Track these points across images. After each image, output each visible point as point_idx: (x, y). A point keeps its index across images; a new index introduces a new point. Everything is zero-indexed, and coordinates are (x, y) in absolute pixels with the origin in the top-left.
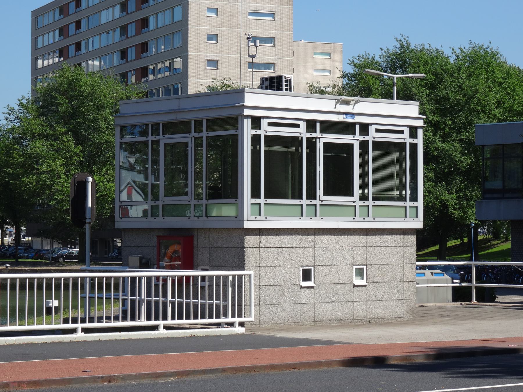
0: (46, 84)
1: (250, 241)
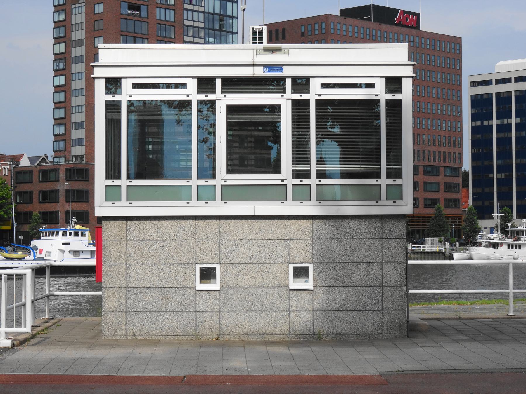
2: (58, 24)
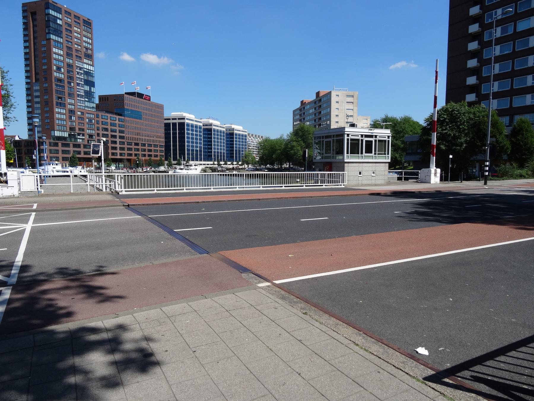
0: (296, 129)
1: (346, 165)
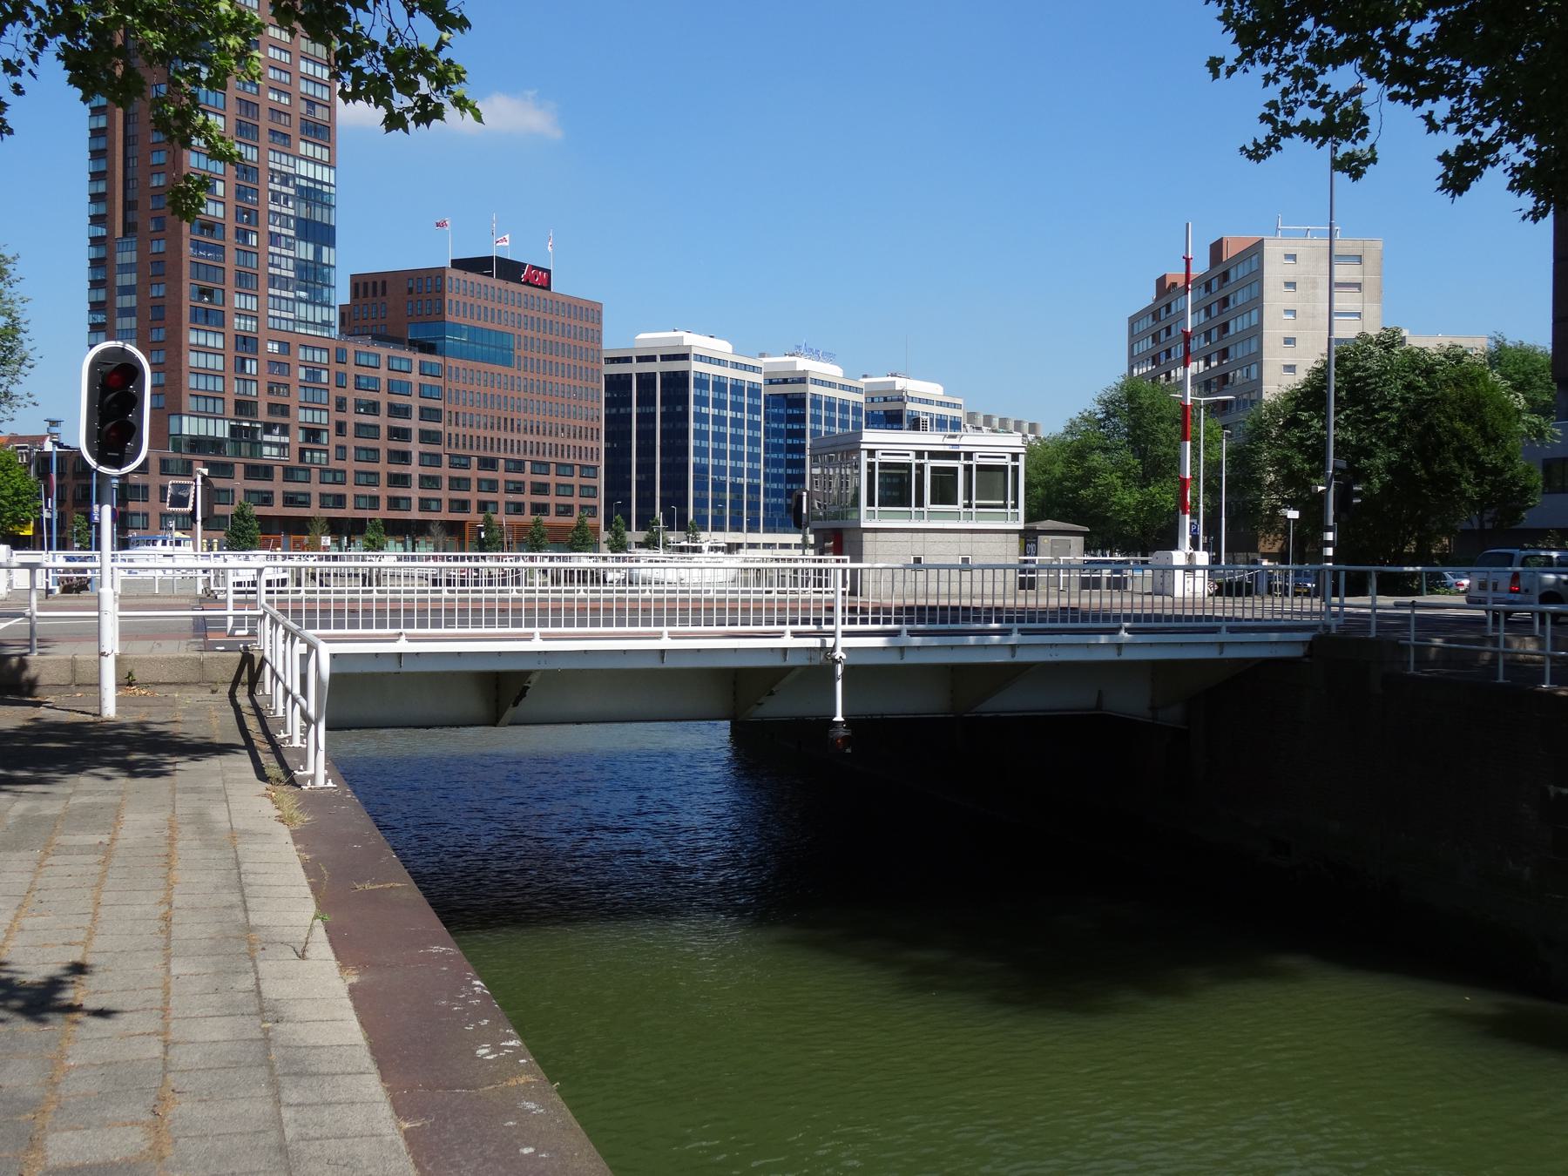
1: (867, 536)
2: (95, 263)
